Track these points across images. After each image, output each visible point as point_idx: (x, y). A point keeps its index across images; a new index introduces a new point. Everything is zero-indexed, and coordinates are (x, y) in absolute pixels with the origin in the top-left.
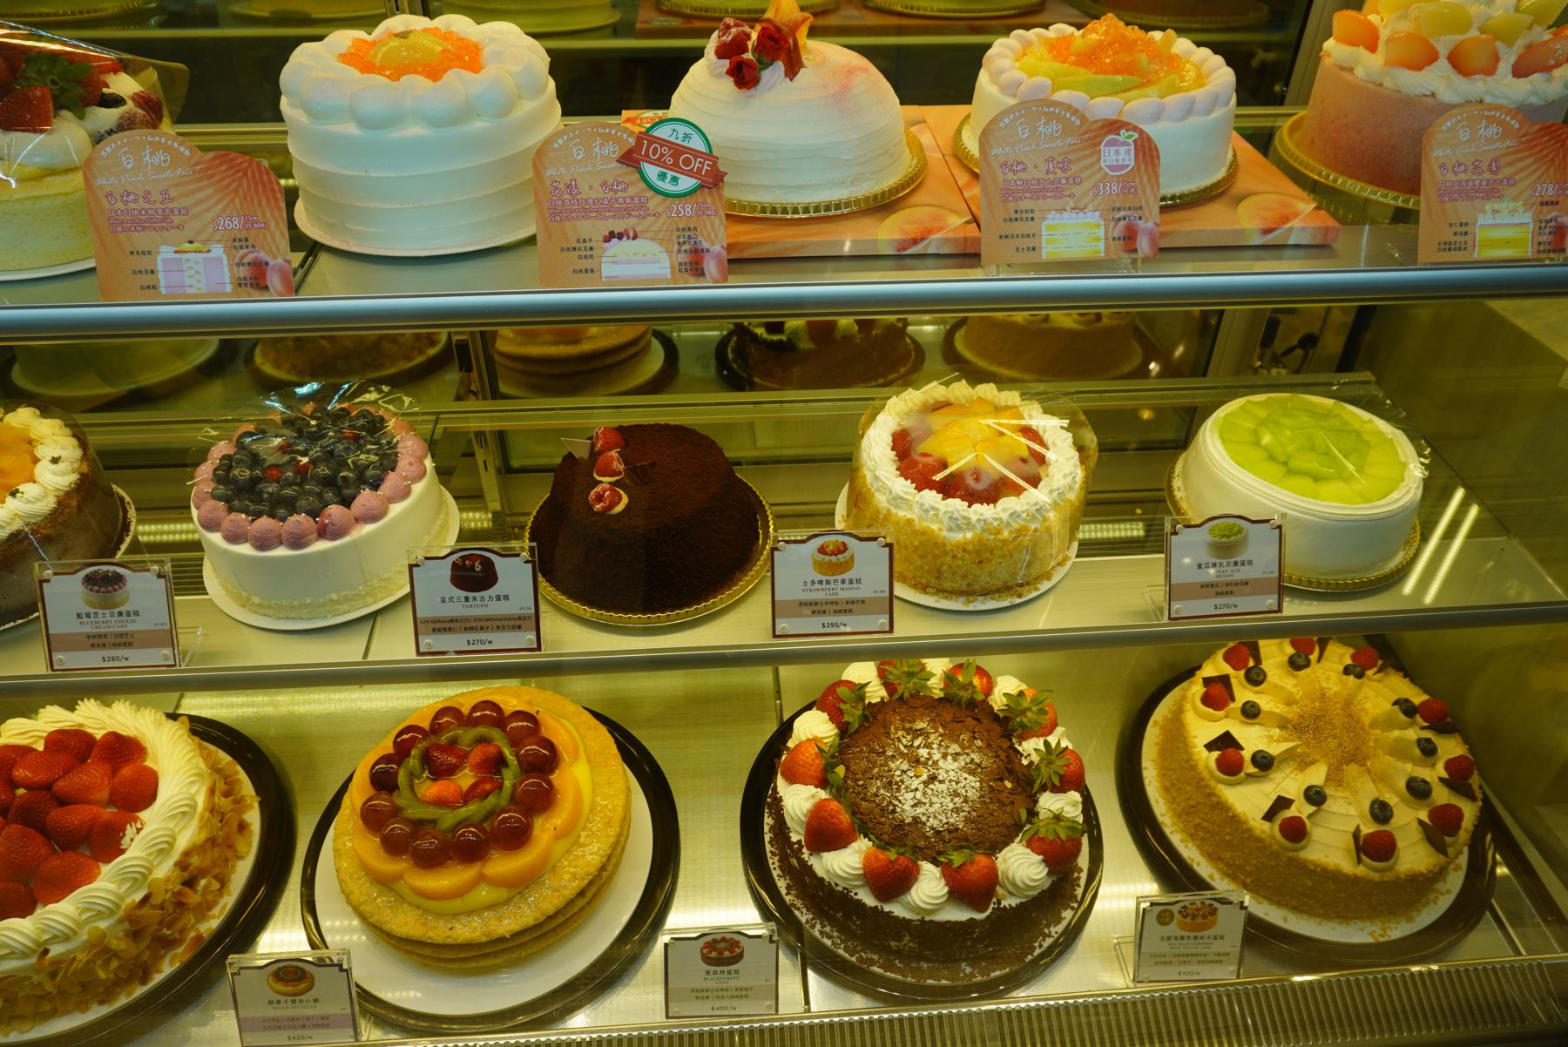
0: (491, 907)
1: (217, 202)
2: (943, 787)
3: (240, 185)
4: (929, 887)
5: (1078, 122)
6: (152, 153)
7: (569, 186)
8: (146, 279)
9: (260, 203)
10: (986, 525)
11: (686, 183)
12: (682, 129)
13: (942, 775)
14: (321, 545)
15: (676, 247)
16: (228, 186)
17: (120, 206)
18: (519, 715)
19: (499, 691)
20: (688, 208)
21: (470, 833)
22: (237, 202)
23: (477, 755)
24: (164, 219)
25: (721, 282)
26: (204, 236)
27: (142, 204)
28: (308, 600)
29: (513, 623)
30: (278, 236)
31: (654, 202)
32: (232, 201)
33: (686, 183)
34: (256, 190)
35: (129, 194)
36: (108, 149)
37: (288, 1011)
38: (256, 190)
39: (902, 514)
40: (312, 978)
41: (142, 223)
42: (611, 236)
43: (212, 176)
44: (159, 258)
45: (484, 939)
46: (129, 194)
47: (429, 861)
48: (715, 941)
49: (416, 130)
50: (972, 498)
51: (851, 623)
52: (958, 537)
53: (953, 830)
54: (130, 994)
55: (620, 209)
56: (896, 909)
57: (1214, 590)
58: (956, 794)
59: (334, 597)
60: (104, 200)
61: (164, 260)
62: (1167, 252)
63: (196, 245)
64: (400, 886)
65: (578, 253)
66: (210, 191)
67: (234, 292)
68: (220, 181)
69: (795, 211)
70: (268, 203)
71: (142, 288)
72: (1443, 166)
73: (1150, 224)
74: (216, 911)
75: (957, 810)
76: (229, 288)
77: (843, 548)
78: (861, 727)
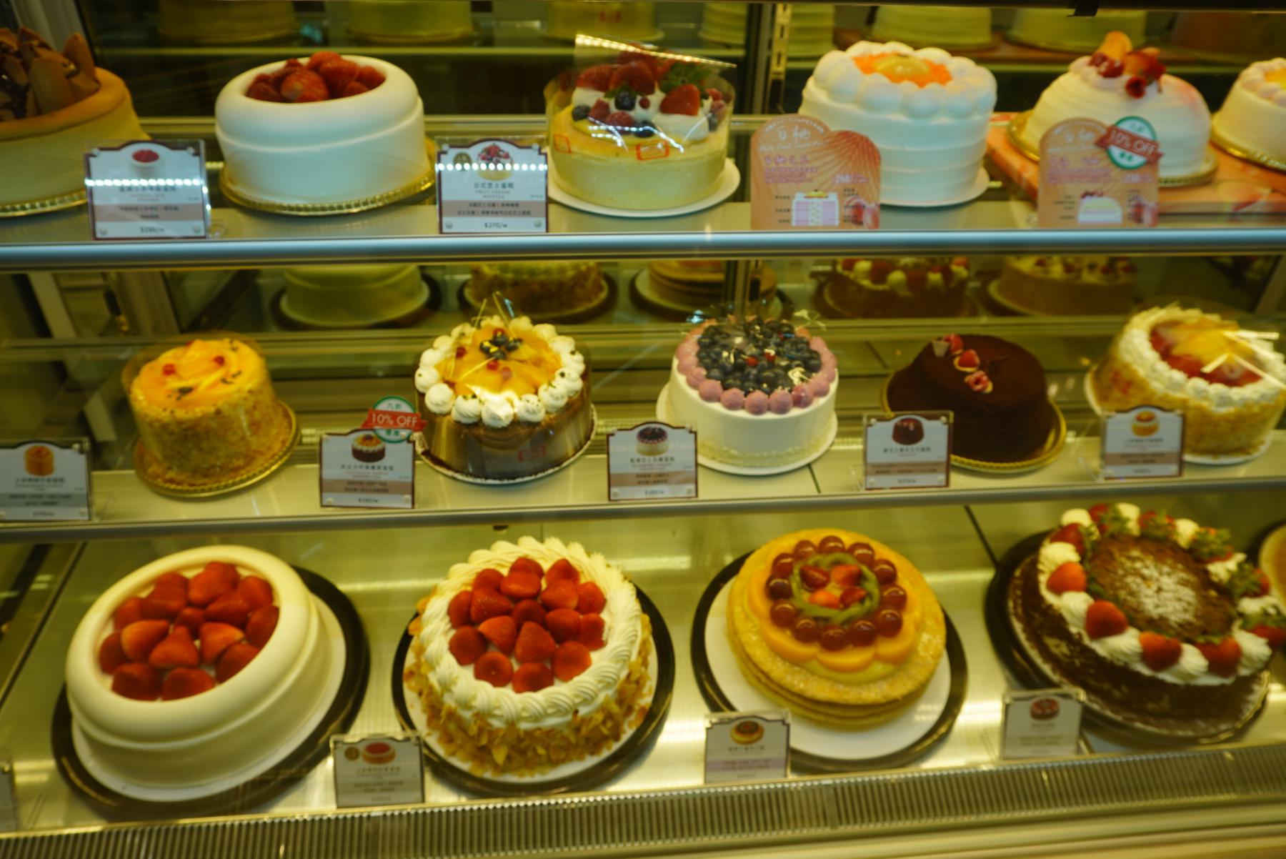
0: (884, 678)
2: (1169, 595)
4: (1192, 660)
7: (1062, 160)
8: (783, 216)
10: (1246, 403)
11: (1138, 160)
12: (1138, 124)
13: (1165, 587)
14: (795, 412)
18: (858, 545)
20: (1136, 178)
21: (864, 625)
23: (839, 574)
24: (802, 174)
25: (1153, 226)
26: (826, 187)
27: (788, 165)
28: (774, 453)
29: (930, 468)
31: (1115, 172)
33: (1138, 160)
37: (743, 755)
39: (1179, 395)
40: (762, 730)
41: (787, 177)
42: (1087, 194)
44: (794, 202)
45: (884, 701)
47: (833, 645)
48: (1041, 702)
49: (943, 120)
50: (1231, 383)
52: (1224, 410)
53: (1189, 624)
54: (609, 748)
56: (1167, 677)
58: (1179, 600)
59: (790, 450)
61: (798, 204)
62: (1163, 216)
63: (819, 193)
64: (814, 665)
66: (833, 157)
67: (841, 226)
71: (1062, 218)
72: (767, 158)
74: (645, 690)
75: (1186, 611)
76: (837, 223)
77: (1150, 419)
78: (1099, 554)
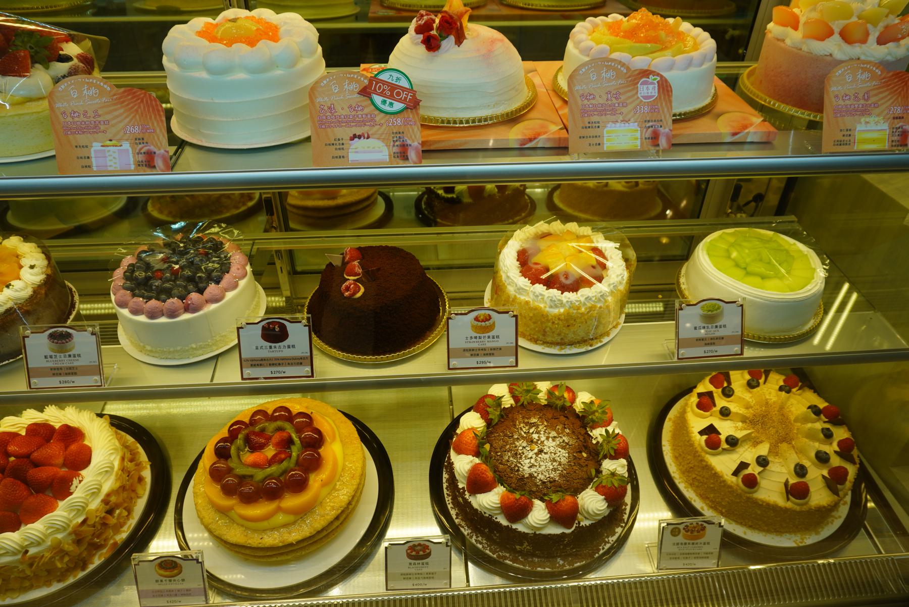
0: (285, 526)
1: (126, 117)
2: (546, 456)
3: (139, 107)
4: (539, 514)
5: (625, 71)
6: (88, 89)
7: (330, 108)
8: (85, 162)
9: (151, 118)
10: (571, 304)
11: (398, 106)
12: (395, 75)
13: (546, 450)
14: (186, 316)
15: (392, 143)
16: (132, 108)
17: (69, 119)
18: (301, 414)
19: (289, 400)
20: (399, 121)
21: (273, 483)
22: (137, 117)
23: (276, 438)
24: (95, 127)
25: (418, 163)
26: (118, 137)
27: (82, 118)
28: (179, 348)
29: (298, 361)
30: (161, 137)
31: (379, 117)
32: (134, 117)
33: (398, 106)
34: (149, 110)
35: (75, 112)
36: (63, 87)
37: (167, 586)
38: (149, 110)
39: (523, 298)
40: (181, 567)
41: (82, 129)
42: (354, 137)
43: (123, 102)
44: (92, 150)
45: (281, 544)
46: (75, 112)
47: (249, 499)
48: (414, 545)
49: (241, 76)
50: (564, 288)
51: (493, 361)
52: (556, 311)
53: (552, 481)
54: (75, 576)
55: (359, 121)
56: (520, 527)
57: (704, 342)
58: (554, 460)
59: (194, 346)
60: (60, 116)
61: (95, 151)
62: (677, 146)
63: (113, 142)
64: (232, 514)
65: (335, 147)
66: (122, 111)
67: (136, 169)
68: (128, 105)
69: (461, 122)
70: (155, 118)
71: (83, 167)
72: (836, 96)
73: (667, 130)
74: (125, 528)
75: (555, 470)
76: (133, 167)
77: (489, 318)
78: (499, 422)
